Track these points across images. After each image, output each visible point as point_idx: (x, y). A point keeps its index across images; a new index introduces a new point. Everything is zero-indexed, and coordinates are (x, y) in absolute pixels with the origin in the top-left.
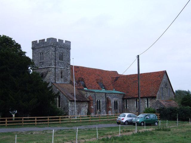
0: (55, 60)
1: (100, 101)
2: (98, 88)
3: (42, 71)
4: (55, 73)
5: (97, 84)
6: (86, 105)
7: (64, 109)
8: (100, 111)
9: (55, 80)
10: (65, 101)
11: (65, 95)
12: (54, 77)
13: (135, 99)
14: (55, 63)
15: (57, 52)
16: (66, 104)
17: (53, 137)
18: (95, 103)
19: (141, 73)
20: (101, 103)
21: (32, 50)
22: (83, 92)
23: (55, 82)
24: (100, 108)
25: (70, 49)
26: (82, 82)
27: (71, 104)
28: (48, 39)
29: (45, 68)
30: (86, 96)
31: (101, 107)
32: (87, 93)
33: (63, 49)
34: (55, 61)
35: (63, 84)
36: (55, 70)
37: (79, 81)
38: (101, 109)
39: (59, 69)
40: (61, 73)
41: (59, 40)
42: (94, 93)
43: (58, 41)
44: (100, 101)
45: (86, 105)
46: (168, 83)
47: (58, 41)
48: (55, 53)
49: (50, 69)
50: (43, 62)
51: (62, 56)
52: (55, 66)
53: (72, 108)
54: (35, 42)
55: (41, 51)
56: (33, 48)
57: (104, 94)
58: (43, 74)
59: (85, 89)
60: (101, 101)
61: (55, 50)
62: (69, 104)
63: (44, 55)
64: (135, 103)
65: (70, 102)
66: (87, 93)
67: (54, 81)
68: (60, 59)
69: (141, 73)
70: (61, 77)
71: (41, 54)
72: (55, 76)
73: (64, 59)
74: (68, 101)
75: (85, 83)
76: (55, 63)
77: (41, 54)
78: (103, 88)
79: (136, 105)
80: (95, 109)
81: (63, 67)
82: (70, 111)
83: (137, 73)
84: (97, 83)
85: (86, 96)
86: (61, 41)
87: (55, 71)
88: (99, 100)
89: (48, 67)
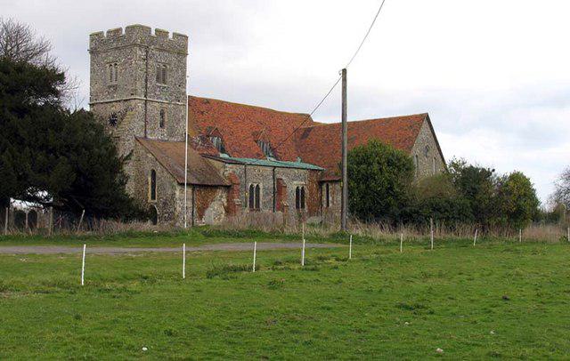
0: (146, 81)
5: (254, 143)
9: (146, 132)
11: (167, 170)
15: (151, 62)
20: (261, 193)
28: (131, 29)
32: (225, 167)
39: (156, 104)
40: (162, 114)
43: (153, 33)
47: (153, 33)
49: (133, 103)
59: (222, 155)
60: (261, 186)
66: (225, 167)
70: (162, 125)
73: (169, 80)
81: (166, 100)
87: (146, 109)
88: (255, 185)
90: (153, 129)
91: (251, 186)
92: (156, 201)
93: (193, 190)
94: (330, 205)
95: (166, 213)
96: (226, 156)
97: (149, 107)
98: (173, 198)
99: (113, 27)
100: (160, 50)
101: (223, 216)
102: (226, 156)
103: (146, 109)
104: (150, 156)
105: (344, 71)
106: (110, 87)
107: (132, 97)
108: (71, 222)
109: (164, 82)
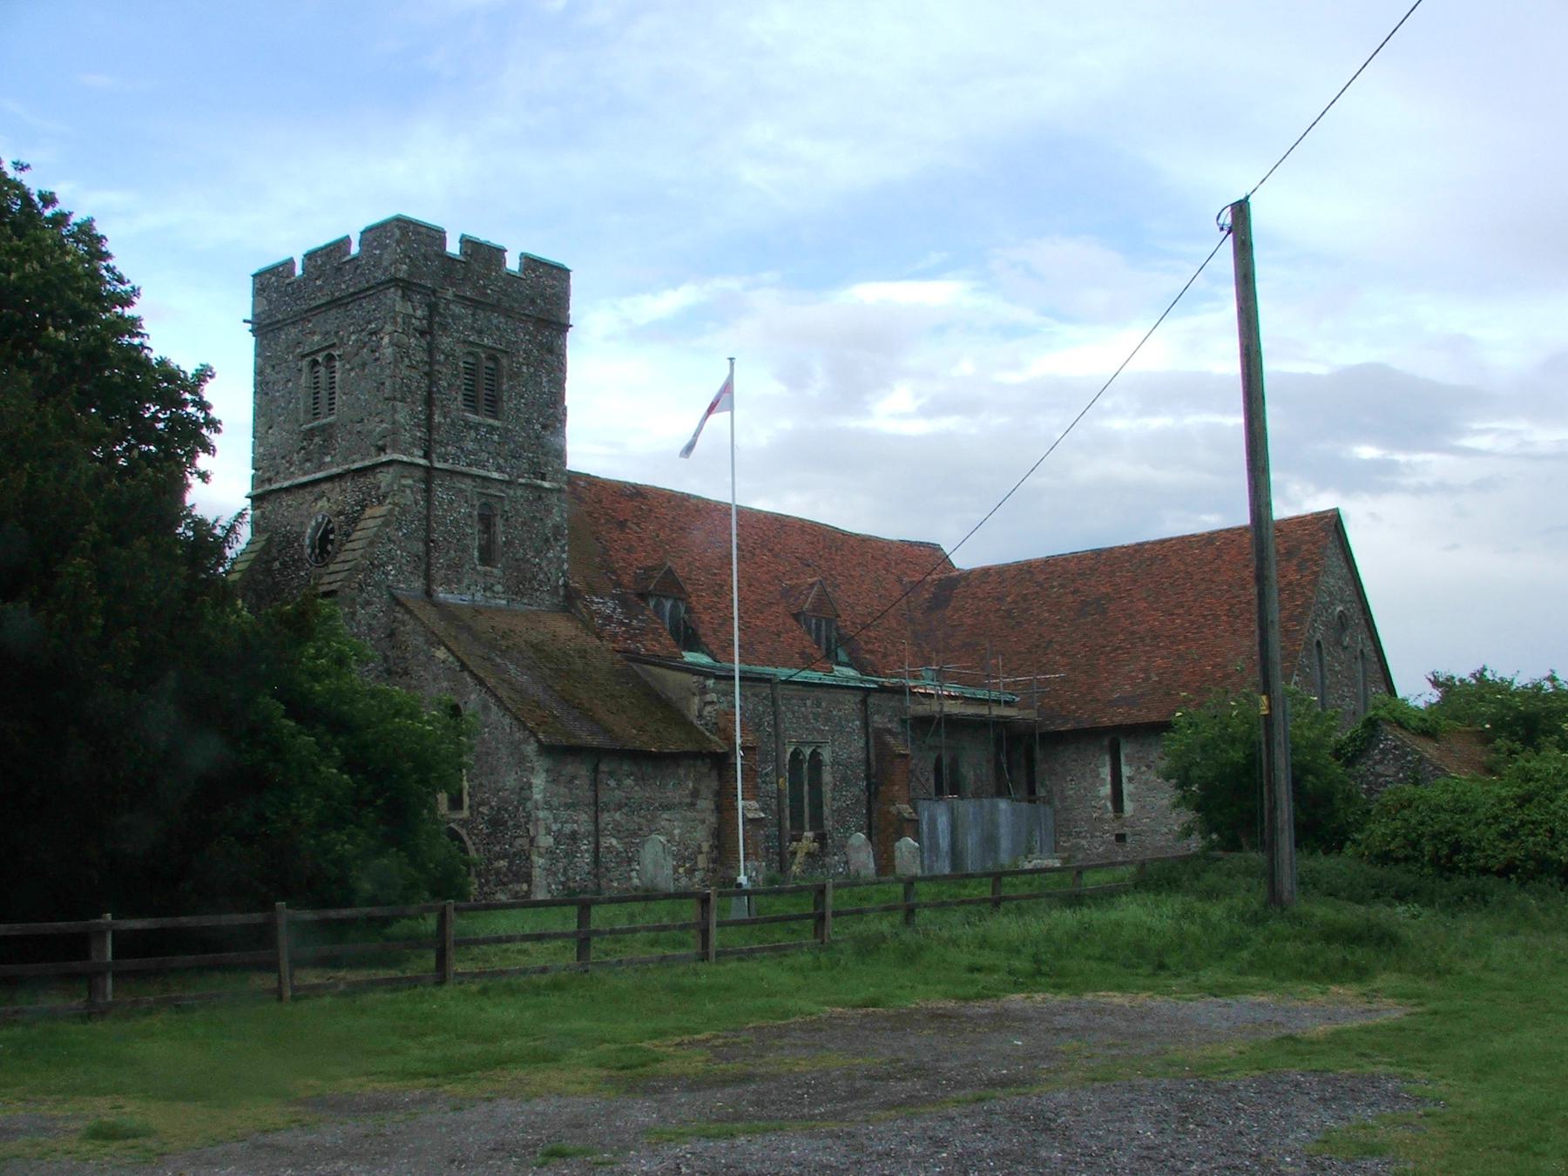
0: (429, 402)
1: (815, 754)
2: (802, 654)
3: (323, 503)
4: (427, 518)
5: (791, 622)
6: (695, 794)
7: (496, 823)
8: (821, 838)
9: (428, 578)
10: (504, 752)
11: (499, 700)
12: (420, 547)
13: (1106, 742)
14: (429, 426)
15: (445, 342)
16: (511, 781)
17: (736, 629)
18: (778, 777)
19: (1281, 510)
20: (827, 777)
21: (249, 342)
22: (674, 680)
23: (429, 593)
24: (817, 821)
25: (563, 327)
26: (668, 604)
27: (554, 778)
28: (374, 235)
29: (340, 476)
30: (700, 716)
31: (826, 811)
32: (704, 690)
33: (496, 319)
34: (430, 418)
35: (499, 610)
36: (428, 490)
37: (643, 596)
38: (829, 824)
39: (466, 485)
40: (486, 521)
41: (466, 241)
42: (765, 690)
43: (453, 248)
44: (815, 754)
45: (695, 794)
46: (1357, 618)
47: (453, 248)
48: (431, 350)
49: (385, 478)
50: (331, 425)
51: (494, 375)
52: (426, 456)
53: (564, 814)
54: (273, 271)
55: (316, 338)
56: (263, 328)
57: (850, 703)
58: (327, 532)
59: (690, 657)
60: (826, 755)
61: (430, 318)
62: (539, 781)
63: (337, 364)
64: (1106, 772)
65: (540, 764)
66: (704, 690)
67: (418, 584)
68: (471, 402)
69: (1281, 510)
70: (487, 556)
71: (315, 363)
72: (428, 541)
73: (508, 405)
74: (531, 749)
75: (689, 610)
76: (429, 426)
77: (315, 363)
78: (843, 657)
79: (1106, 790)
80: (780, 826)
81: (499, 469)
82: (546, 841)
83: (1243, 518)
84: (796, 617)
85: (700, 716)
86: (483, 255)
87: (428, 500)
88: (808, 751)
89: (367, 463)
90: (455, 567)
91: (795, 754)
92: (465, 813)
93: (596, 770)
94: (1128, 806)
95: (498, 858)
96: (702, 659)
97: (439, 493)
98: (524, 800)
99: (321, 237)
100: (475, 304)
101: (702, 861)
102: (702, 659)
103: (428, 500)
104: (441, 653)
105: (1241, 210)
106: (310, 434)
107: (384, 458)
108: (1535, 686)
109: (493, 406)
